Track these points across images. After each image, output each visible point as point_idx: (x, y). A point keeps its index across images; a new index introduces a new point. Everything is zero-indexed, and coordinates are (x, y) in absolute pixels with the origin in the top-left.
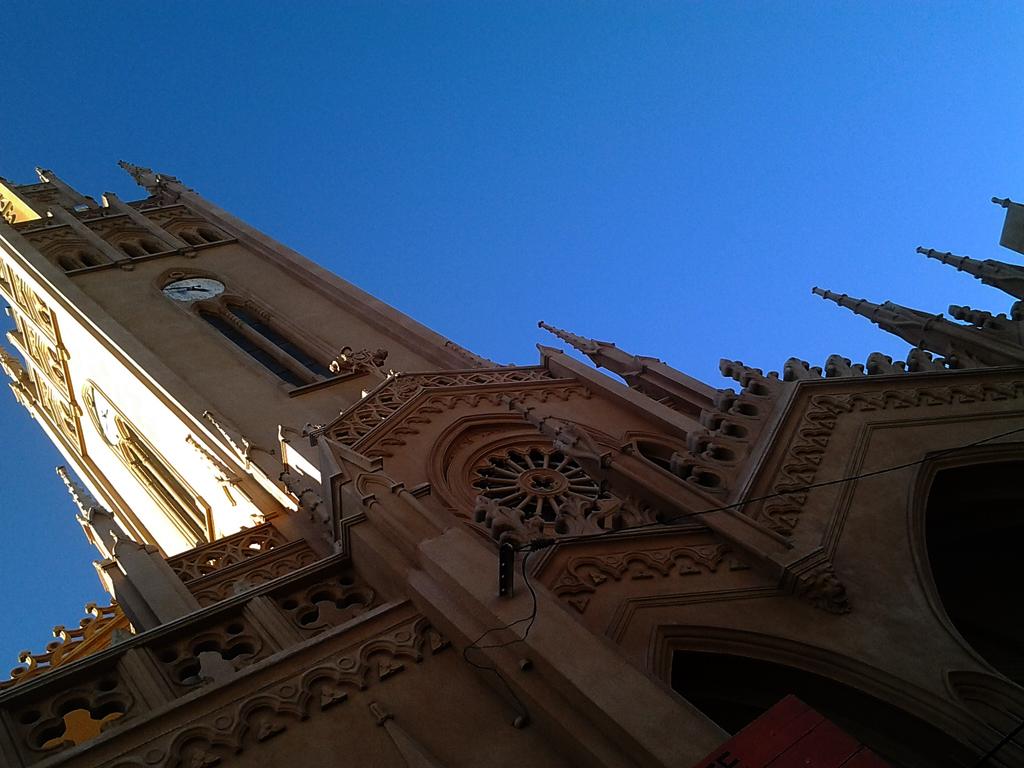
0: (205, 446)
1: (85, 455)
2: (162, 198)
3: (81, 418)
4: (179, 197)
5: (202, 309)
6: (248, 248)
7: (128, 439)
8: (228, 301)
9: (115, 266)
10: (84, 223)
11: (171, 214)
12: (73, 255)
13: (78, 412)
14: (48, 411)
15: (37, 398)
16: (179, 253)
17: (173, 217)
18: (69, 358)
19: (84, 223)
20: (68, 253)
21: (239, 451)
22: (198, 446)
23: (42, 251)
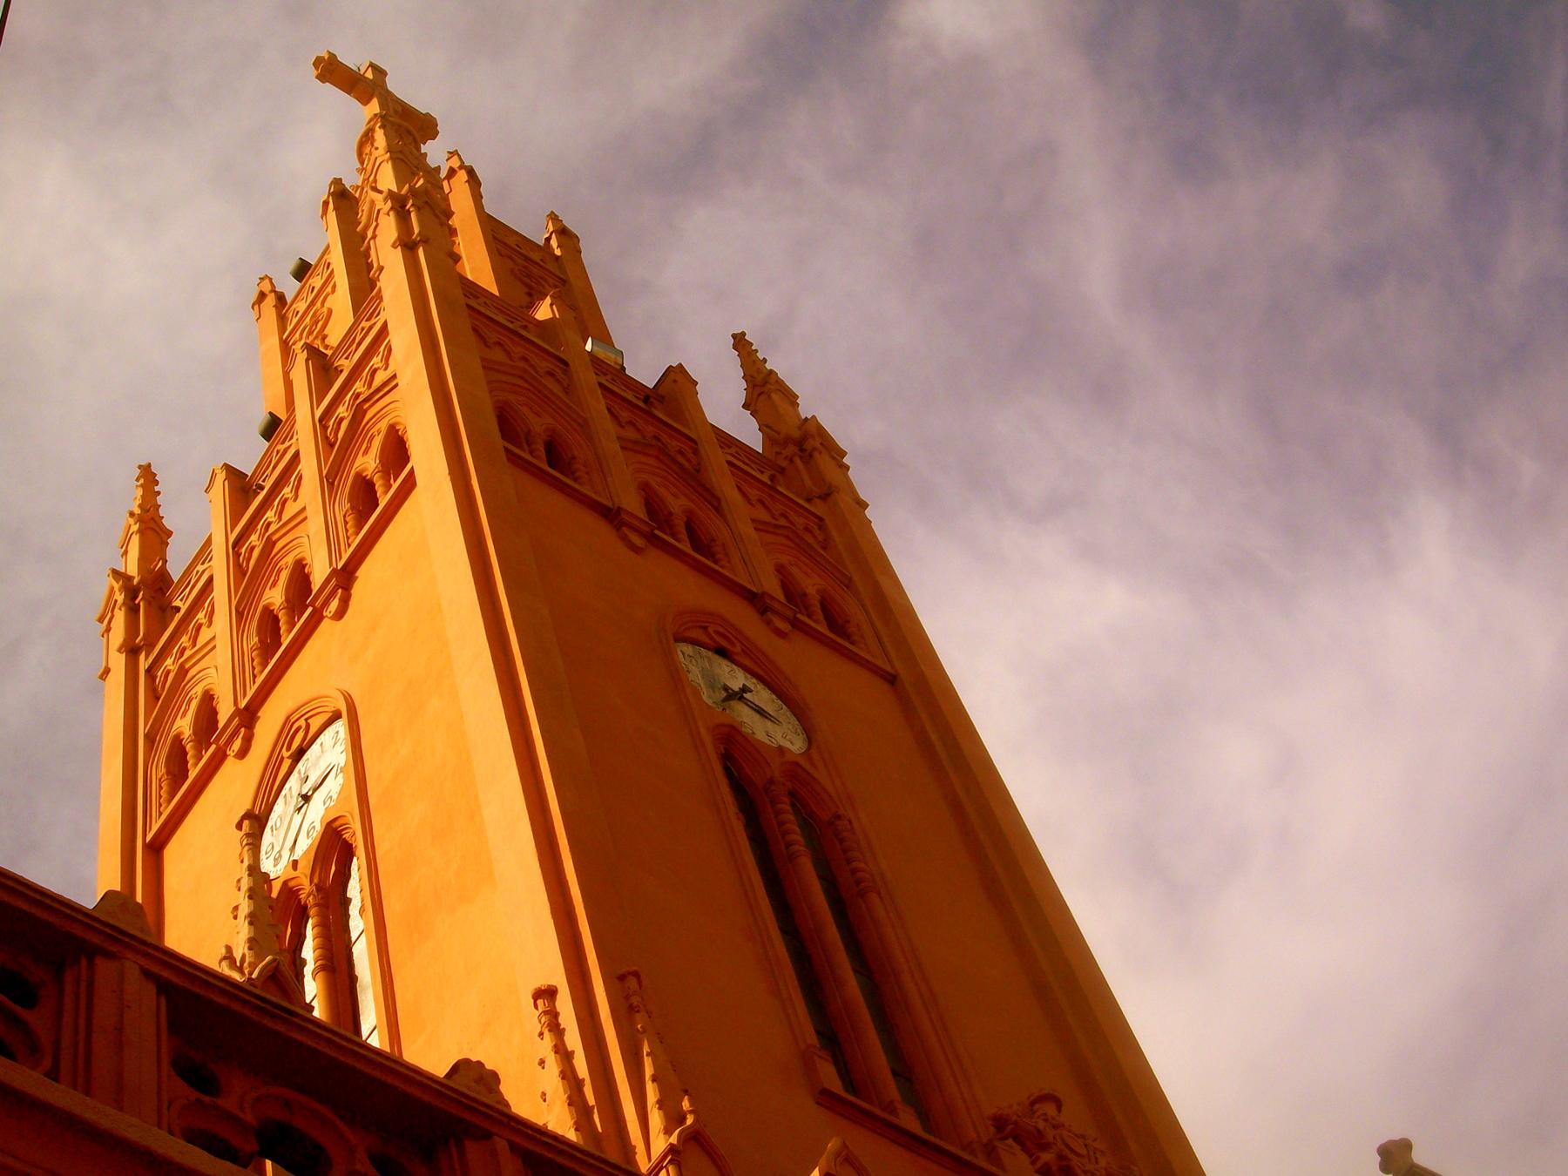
0: (573, 1040)
1: (156, 849)
2: (782, 471)
3: (230, 765)
4: (826, 497)
5: (733, 750)
6: (903, 701)
7: (319, 888)
8: (795, 771)
9: (611, 515)
10: (601, 385)
11: (525, 359)
12: (538, 424)
13: (237, 744)
14: (153, 694)
15: (150, 646)
16: (757, 601)
17: (783, 522)
18: (340, 614)
19: (601, 385)
20: (525, 410)
21: (656, 1119)
22: (556, 1029)
23: (488, 366)
